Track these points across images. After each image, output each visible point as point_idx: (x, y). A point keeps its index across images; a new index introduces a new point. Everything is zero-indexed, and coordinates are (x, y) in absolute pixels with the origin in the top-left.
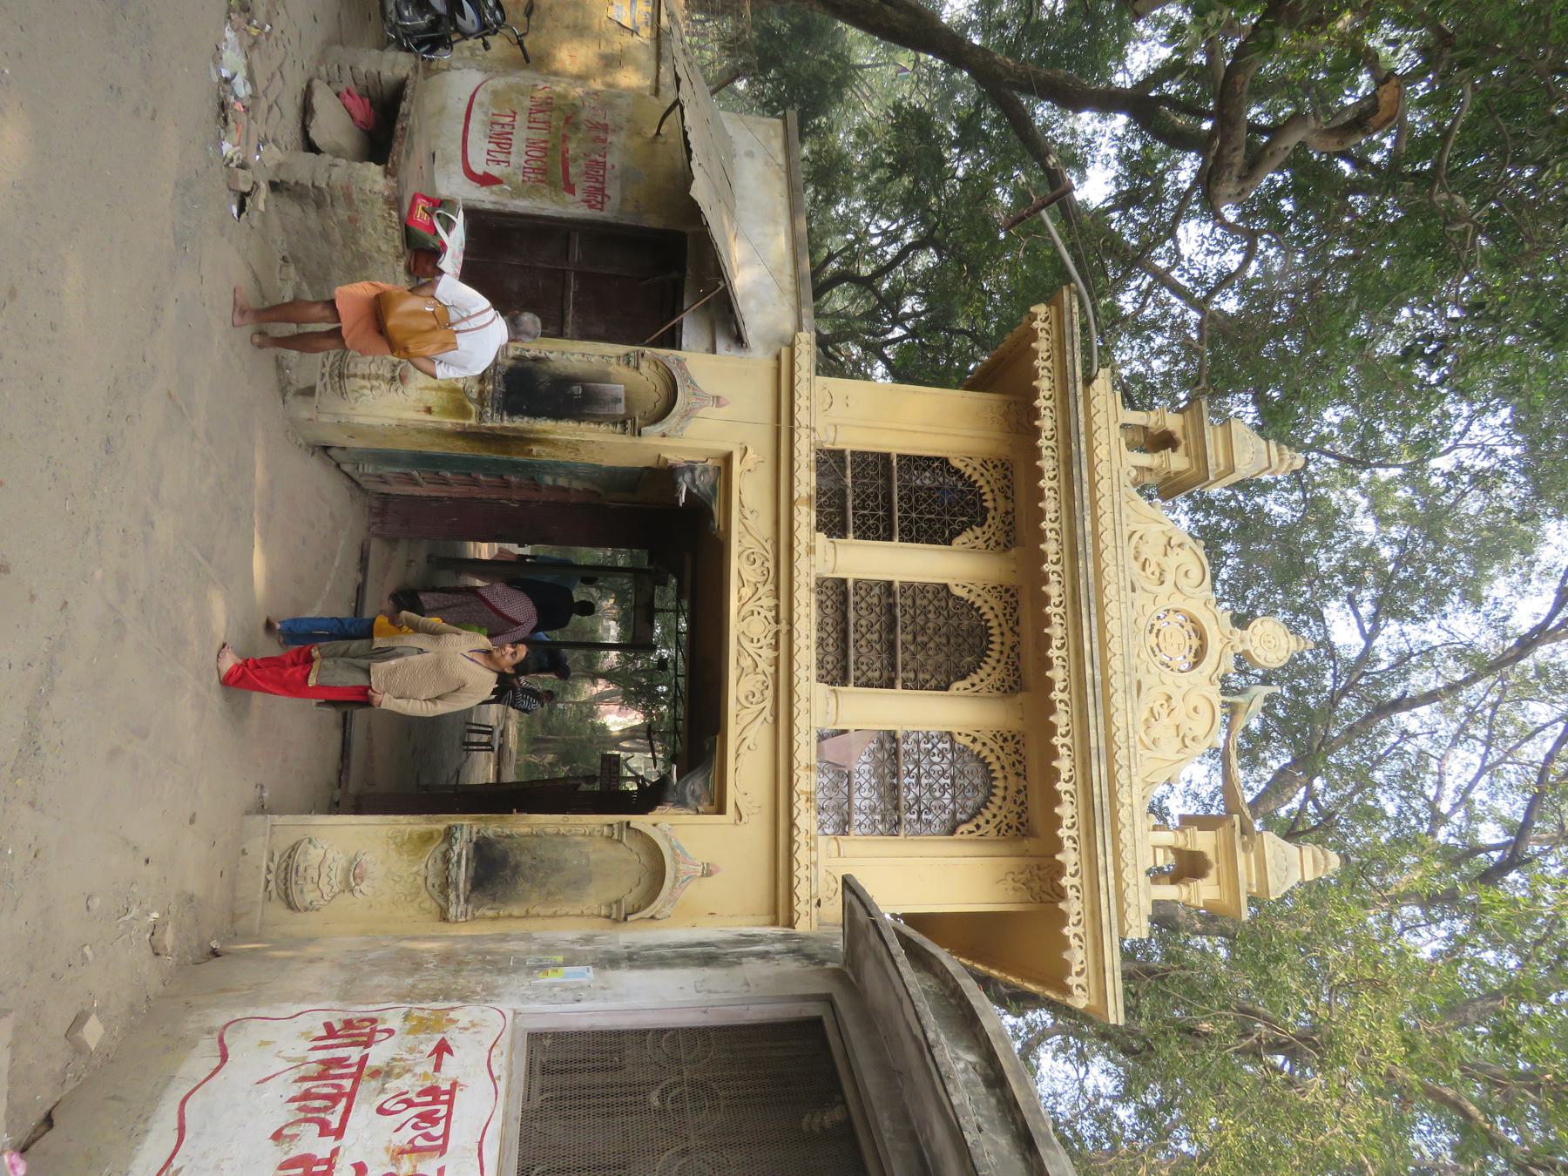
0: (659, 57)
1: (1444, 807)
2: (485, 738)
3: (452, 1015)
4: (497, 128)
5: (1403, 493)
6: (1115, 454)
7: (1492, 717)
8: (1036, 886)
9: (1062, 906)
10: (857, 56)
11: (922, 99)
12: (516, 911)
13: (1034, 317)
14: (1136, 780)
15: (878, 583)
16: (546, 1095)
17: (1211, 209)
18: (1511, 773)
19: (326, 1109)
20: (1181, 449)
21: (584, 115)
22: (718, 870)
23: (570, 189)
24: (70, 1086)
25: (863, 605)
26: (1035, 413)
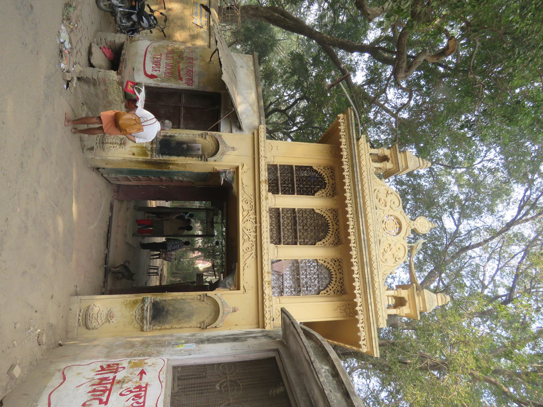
0: (210, 35)
1: (486, 283)
2: (155, 271)
3: (146, 361)
4: (156, 59)
5: (466, 177)
6: (368, 165)
7: (500, 251)
8: (348, 311)
9: (357, 317)
10: (278, 37)
11: (300, 51)
12: (168, 327)
13: (339, 118)
14: (380, 273)
15: (290, 209)
16: (180, 387)
17: (397, 85)
18: (507, 270)
19: (101, 395)
20: (390, 161)
21: (185, 55)
22: (238, 310)
23: (181, 79)
24: (9, 391)
25: (285, 217)
26: (341, 150)
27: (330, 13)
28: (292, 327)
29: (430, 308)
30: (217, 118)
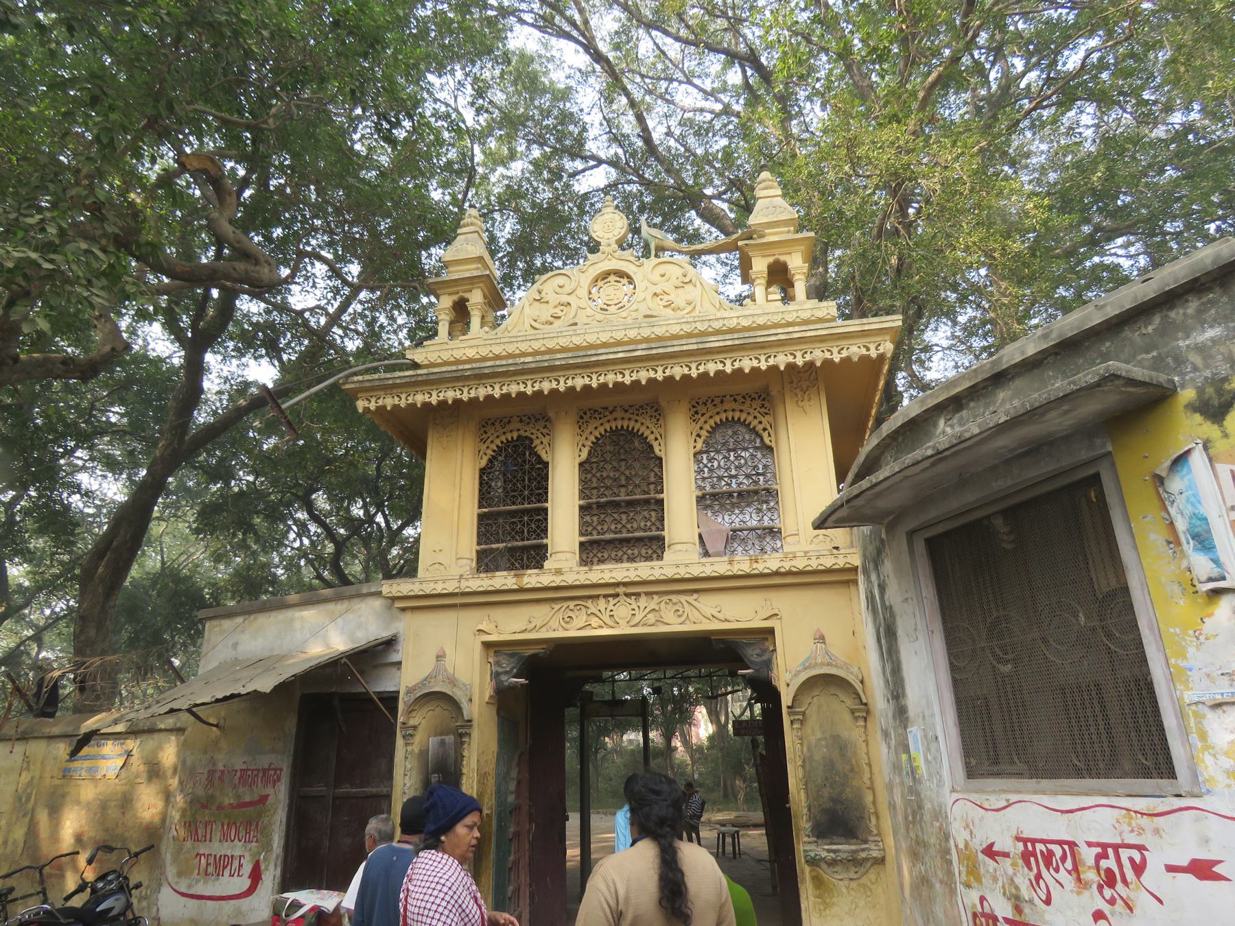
0: (152, 731)
1: (718, 107)
2: (729, 840)
3: (961, 846)
4: (211, 869)
5: (492, 144)
8: (805, 384)
9: (818, 364)
13: (367, 410)
14: (719, 315)
15: (581, 517)
16: (1016, 760)
20: (466, 295)
21: (200, 792)
22: (818, 630)
23: (264, 799)
25: (599, 528)
26: (443, 403)
27: (103, 444)
28: (858, 502)
29: (789, 212)
30: (365, 699)
